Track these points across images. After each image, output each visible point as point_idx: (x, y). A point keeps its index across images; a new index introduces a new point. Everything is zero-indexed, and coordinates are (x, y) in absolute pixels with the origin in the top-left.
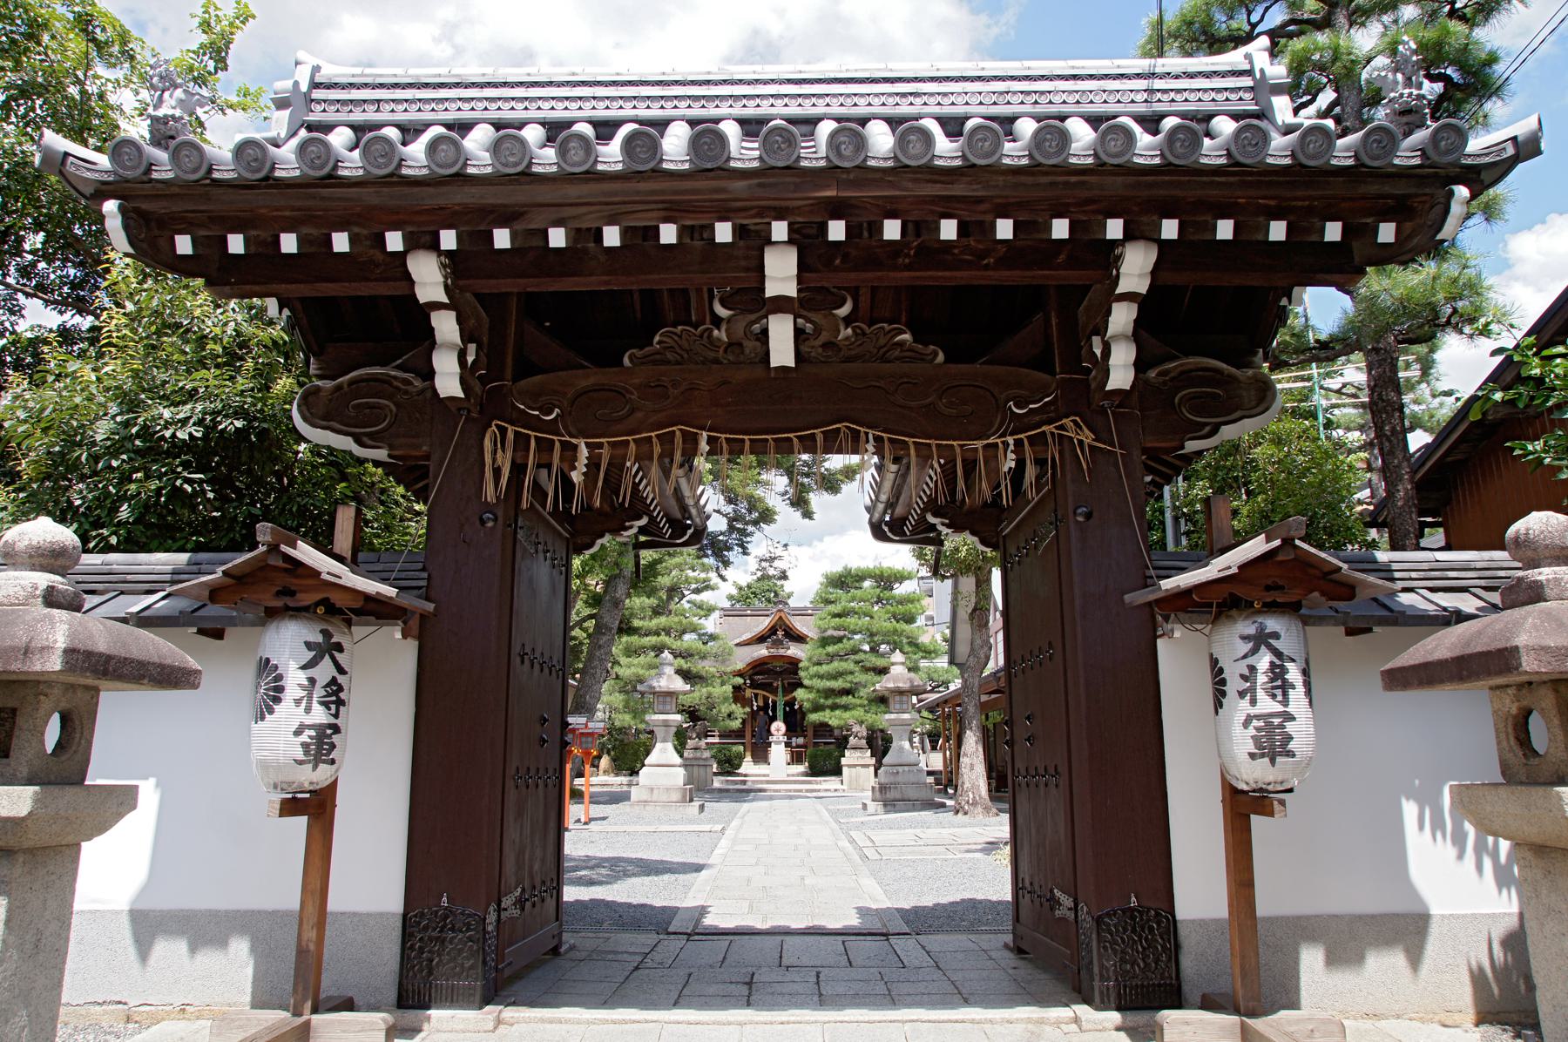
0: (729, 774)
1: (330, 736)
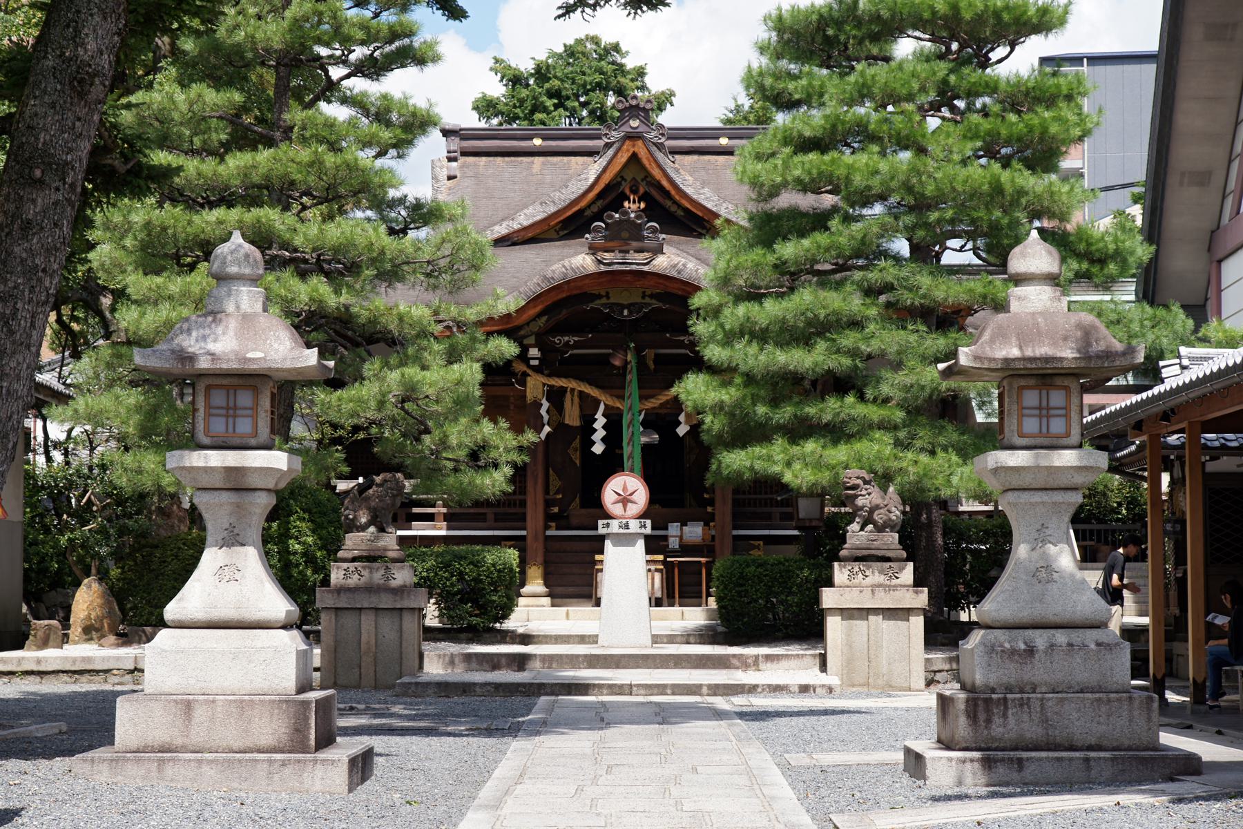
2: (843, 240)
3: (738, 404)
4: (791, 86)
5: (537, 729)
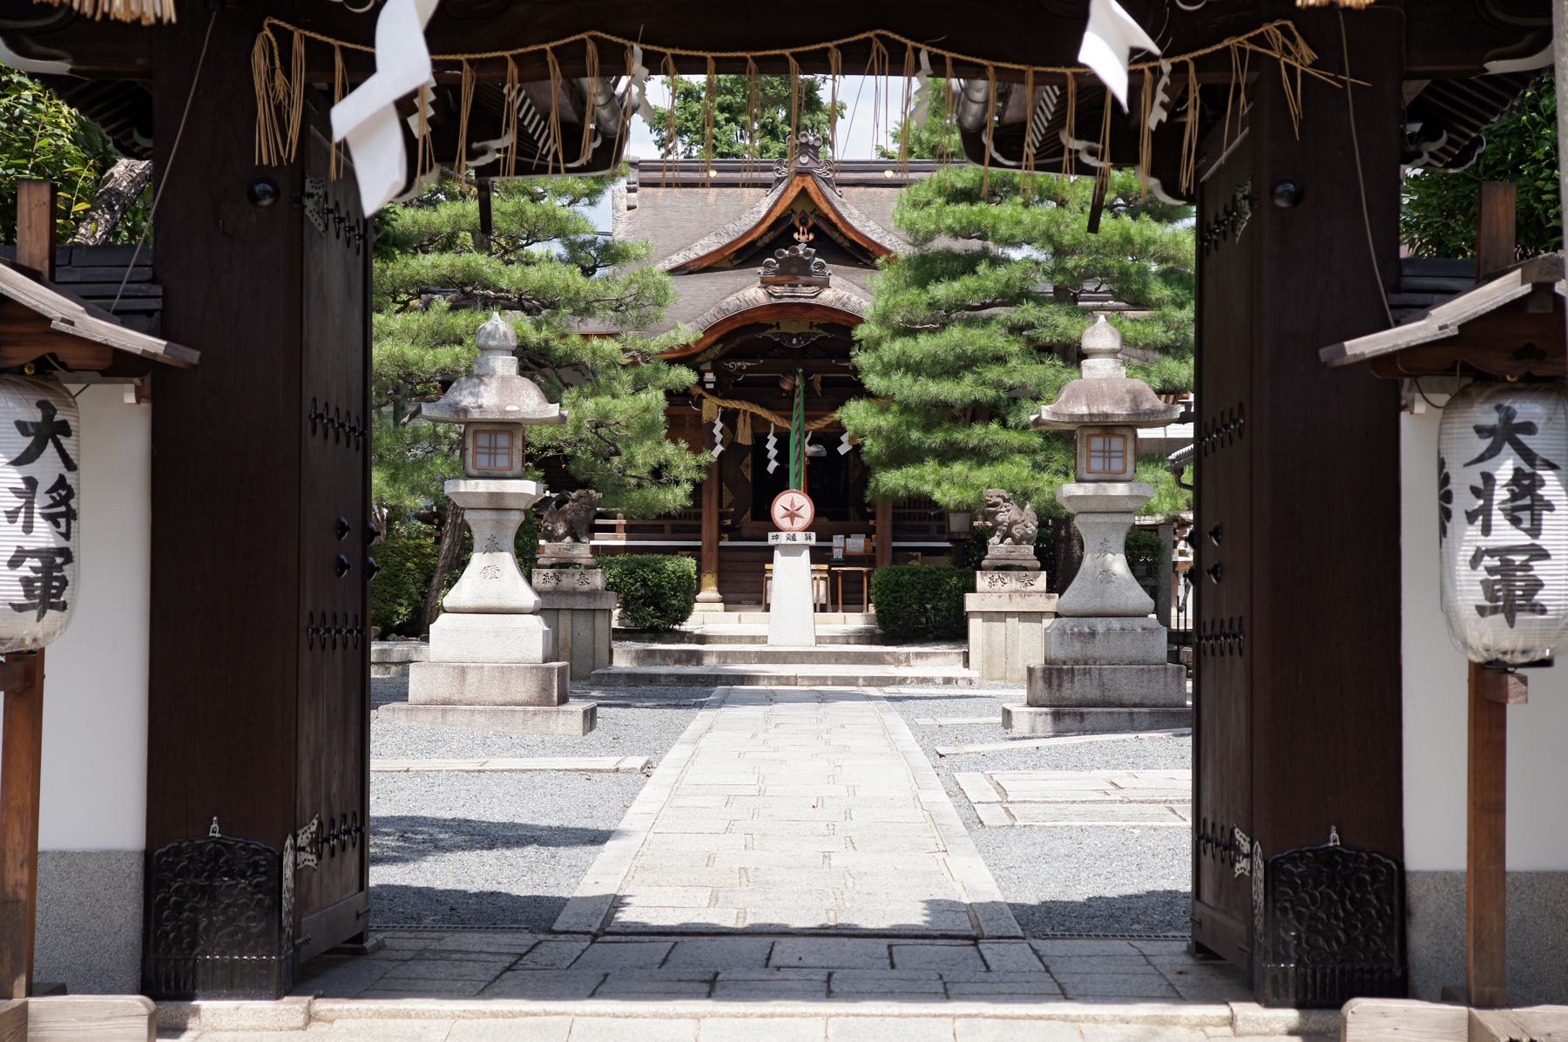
0: (657, 634)
1: (59, 568)
2: (990, 284)
3: (895, 429)
4: (945, 140)
5: (721, 703)
